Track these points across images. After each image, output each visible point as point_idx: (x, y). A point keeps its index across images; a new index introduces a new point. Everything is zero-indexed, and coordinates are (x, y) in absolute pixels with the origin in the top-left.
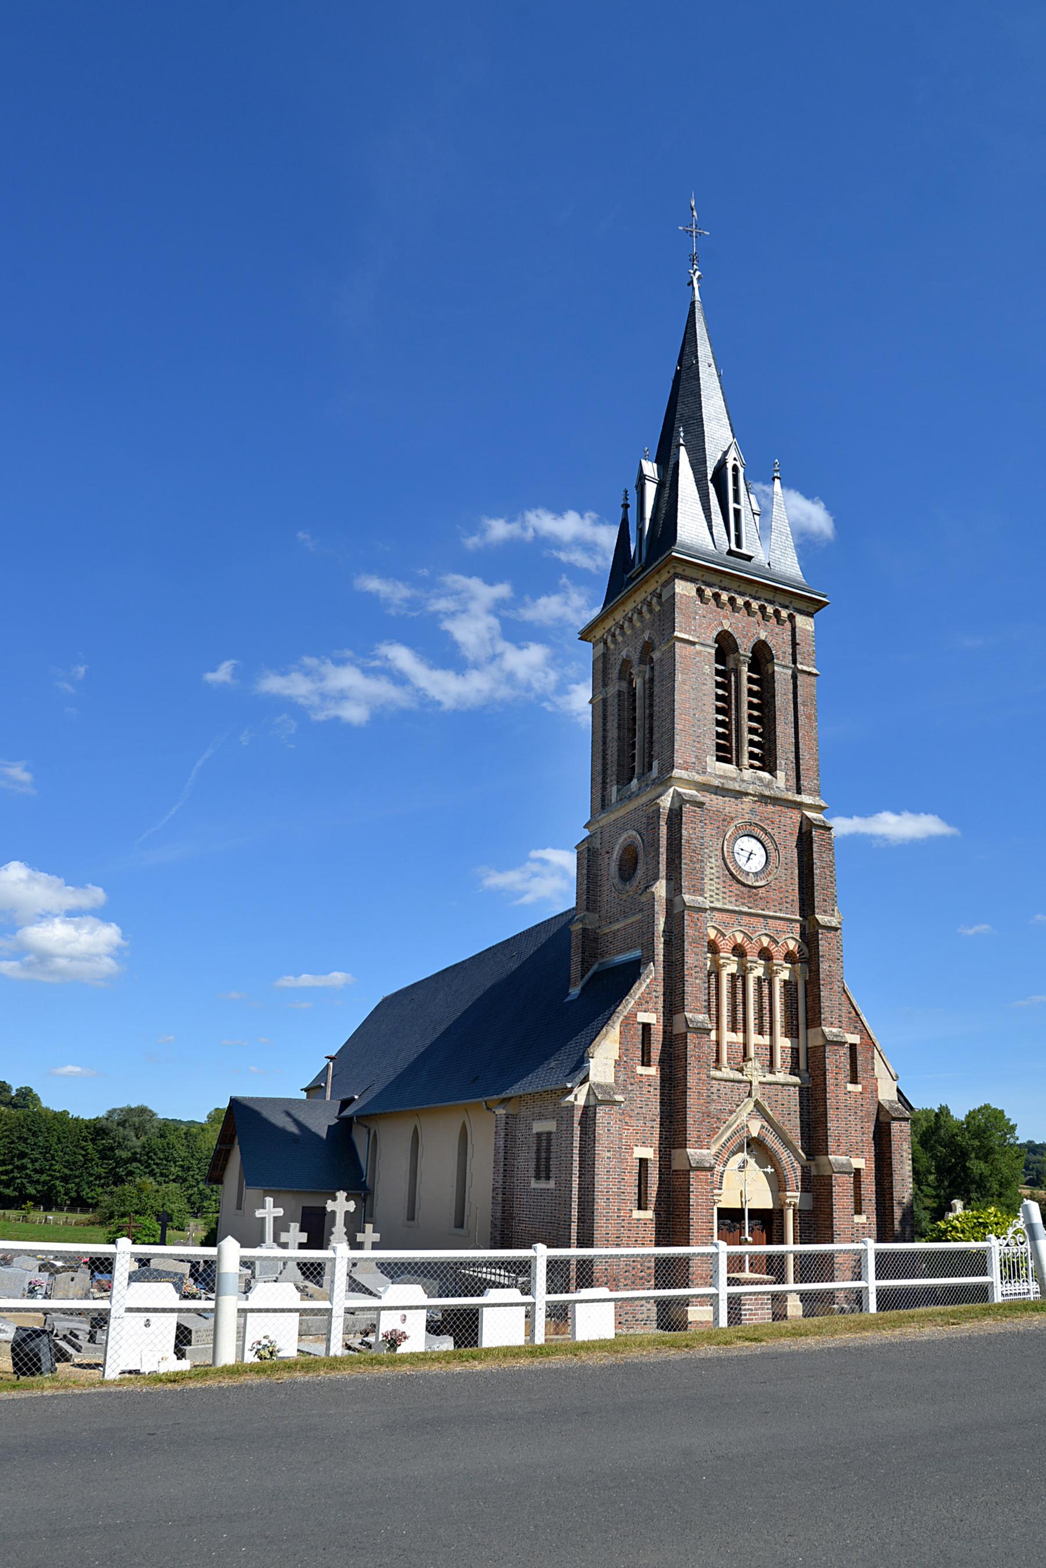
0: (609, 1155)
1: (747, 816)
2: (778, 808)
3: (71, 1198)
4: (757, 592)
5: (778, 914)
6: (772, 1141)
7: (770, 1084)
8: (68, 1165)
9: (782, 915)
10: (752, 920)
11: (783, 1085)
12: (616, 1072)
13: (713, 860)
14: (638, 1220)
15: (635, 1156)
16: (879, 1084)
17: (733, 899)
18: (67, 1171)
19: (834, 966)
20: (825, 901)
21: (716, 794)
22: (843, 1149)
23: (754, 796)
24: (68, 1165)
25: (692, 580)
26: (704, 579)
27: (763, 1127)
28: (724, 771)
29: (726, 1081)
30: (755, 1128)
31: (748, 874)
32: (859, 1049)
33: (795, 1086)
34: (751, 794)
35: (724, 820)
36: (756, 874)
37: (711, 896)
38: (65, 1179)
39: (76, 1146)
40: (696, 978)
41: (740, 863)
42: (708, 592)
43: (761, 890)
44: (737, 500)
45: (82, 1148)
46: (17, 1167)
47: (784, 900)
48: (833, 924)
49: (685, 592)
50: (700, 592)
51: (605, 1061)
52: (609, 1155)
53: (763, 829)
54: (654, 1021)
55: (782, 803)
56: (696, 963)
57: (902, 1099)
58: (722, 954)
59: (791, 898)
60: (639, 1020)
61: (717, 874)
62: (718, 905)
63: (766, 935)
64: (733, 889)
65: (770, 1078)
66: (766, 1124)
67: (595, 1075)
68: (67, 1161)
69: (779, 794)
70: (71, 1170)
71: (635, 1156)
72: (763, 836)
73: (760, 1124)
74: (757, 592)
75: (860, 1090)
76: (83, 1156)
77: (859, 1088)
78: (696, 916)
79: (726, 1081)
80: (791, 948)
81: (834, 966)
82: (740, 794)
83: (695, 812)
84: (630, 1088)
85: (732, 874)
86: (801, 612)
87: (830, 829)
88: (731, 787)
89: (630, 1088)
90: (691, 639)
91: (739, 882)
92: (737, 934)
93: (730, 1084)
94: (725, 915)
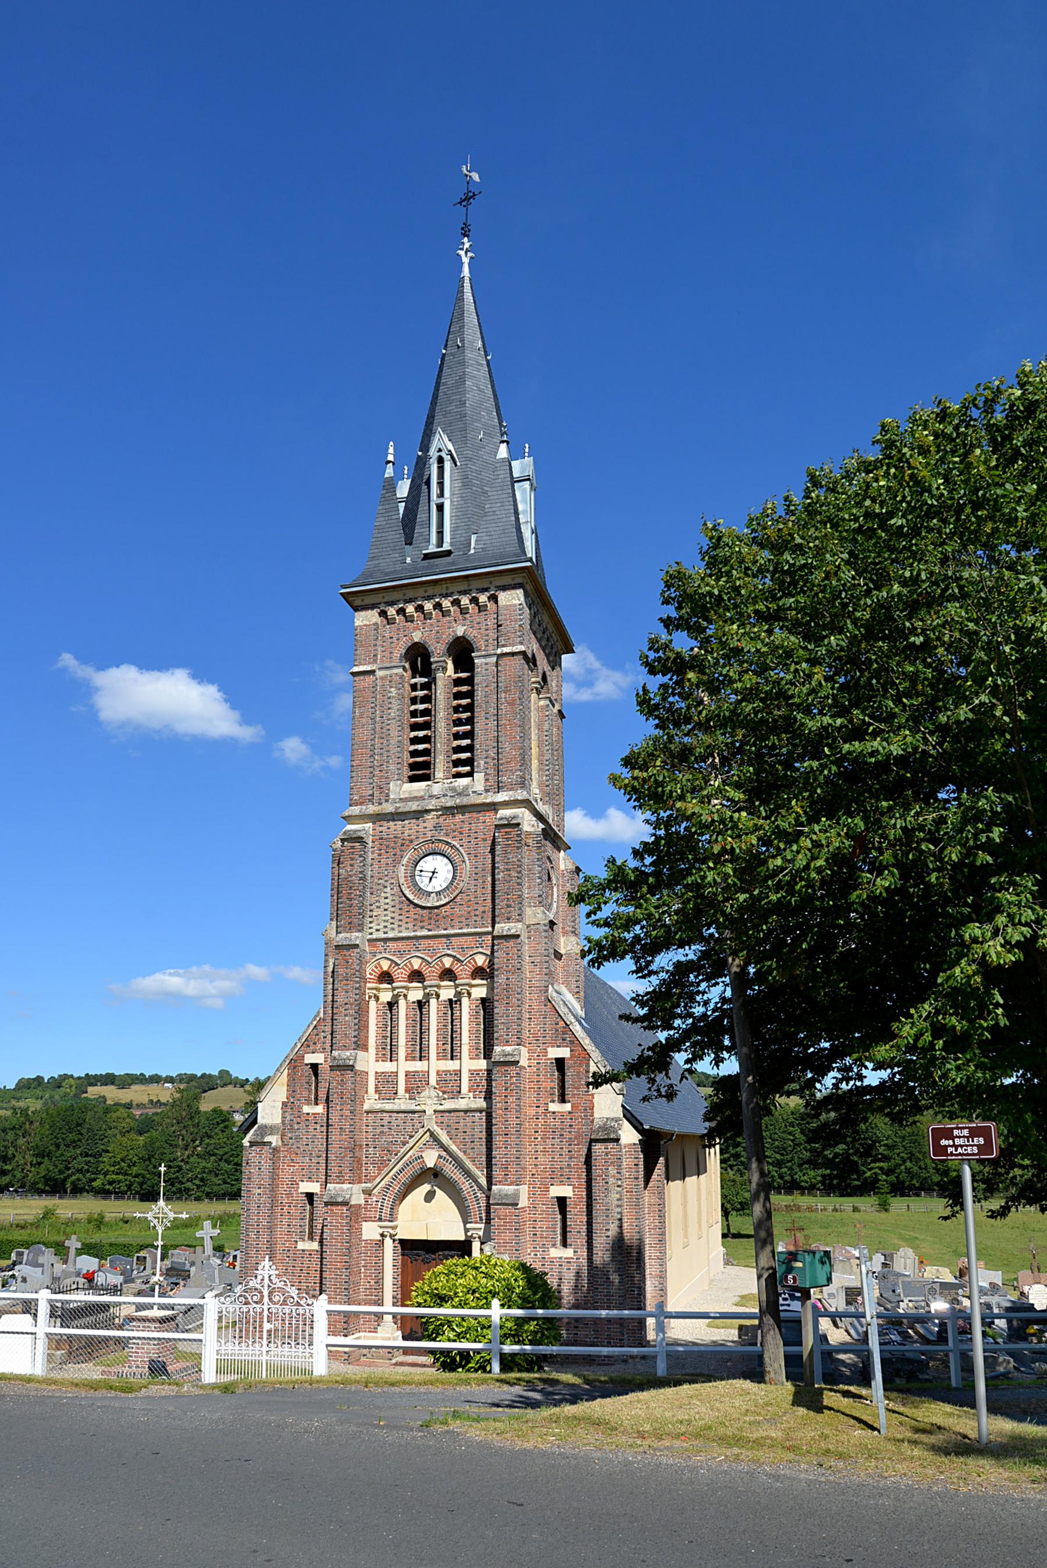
0: (259, 1191)
1: (429, 834)
2: (467, 815)
3: (786, 1182)
4: (447, 588)
5: (465, 931)
6: (450, 1170)
7: (450, 1111)
8: (779, 1150)
9: (473, 930)
10: (431, 942)
11: (466, 1111)
12: (284, 1112)
13: (388, 889)
14: (303, 1250)
15: (300, 1190)
16: (595, 1101)
17: (410, 925)
18: (778, 1156)
19: (513, 978)
20: (509, 906)
21: (394, 820)
22: (512, 1177)
23: (436, 810)
24: (779, 1150)
25: (372, 607)
26: (385, 600)
27: (440, 1157)
28: (410, 792)
29: (398, 1112)
30: (431, 1158)
31: (429, 894)
32: (568, 1064)
33: (481, 1111)
34: (433, 810)
35: (402, 845)
36: (438, 893)
37: (386, 927)
38: (779, 1164)
39: (784, 1132)
40: (346, 1015)
41: (421, 886)
42: (392, 611)
43: (443, 909)
44: (441, 495)
45: (790, 1133)
46: (732, 1155)
47: (472, 914)
48: (513, 932)
49: (365, 622)
50: (383, 614)
51: (272, 1104)
52: (259, 1191)
53: (448, 843)
54: (322, 1061)
55: (472, 809)
56: (346, 1001)
57: (629, 1115)
58: (368, 985)
59: (481, 909)
60: (306, 1062)
61: (392, 903)
62: (391, 935)
63: (449, 955)
64: (411, 914)
65: (449, 1105)
66: (444, 1154)
67: (263, 1117)
68: (778, 1147)
69: (480, 800)
70: (782, 1155)
71: (300, 1190)
72: (449, 851)
73: (437, 1154)
74: (447, 588)
75: (570, 1109)
76: (792, 1141)
77: (568, 1107)
78: (347, 953)
79: (398, 1112)
80: (480, 964)
81: (513, 978)
82: (419, 814)
83: (353, 847)
84: (296, 1126)
85: (408, 899)
86: (504, 588)
87: (518, 824)
88: (407, 809)
89: (296, 1126)
90: (369, 669)
91: (416, 905)
92: (413, 960)
93: (403, 1115)
94: (400, 944)
